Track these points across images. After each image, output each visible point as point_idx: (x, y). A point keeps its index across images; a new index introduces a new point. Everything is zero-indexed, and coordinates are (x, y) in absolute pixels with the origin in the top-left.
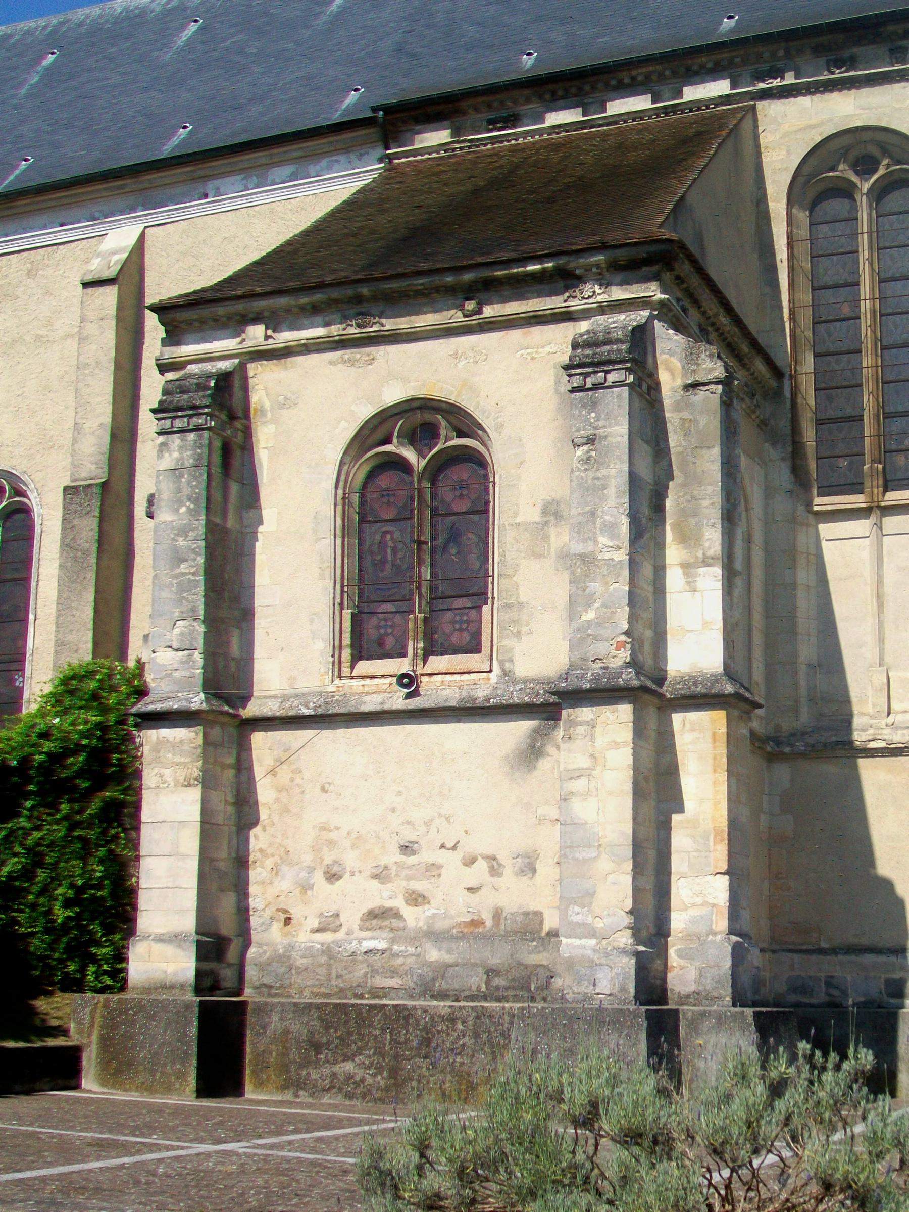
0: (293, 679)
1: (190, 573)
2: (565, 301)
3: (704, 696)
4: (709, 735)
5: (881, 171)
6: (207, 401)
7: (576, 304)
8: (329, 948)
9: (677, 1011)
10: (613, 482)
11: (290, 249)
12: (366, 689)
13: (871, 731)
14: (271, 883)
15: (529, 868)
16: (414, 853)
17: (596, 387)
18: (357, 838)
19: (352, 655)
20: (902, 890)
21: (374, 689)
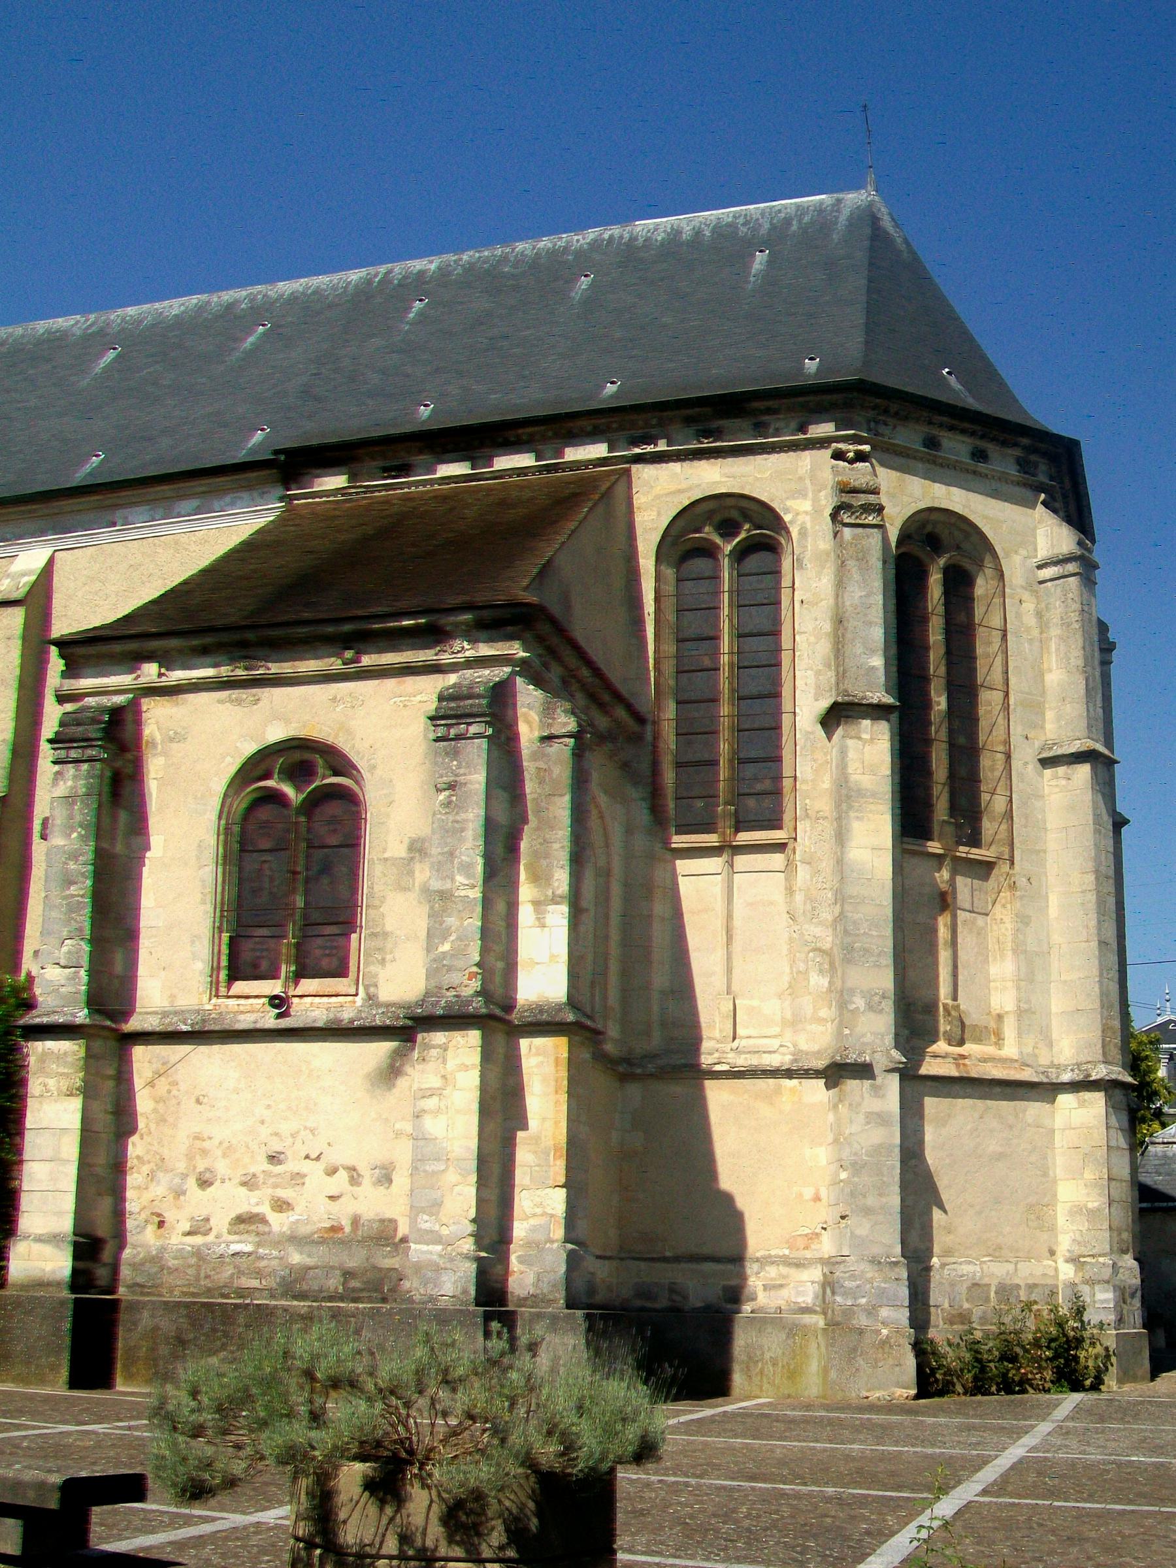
0: (173, 997)
1: (78, 896)
2: (436, 655)
3: (548, 1023)
4: (552, 1060)
5: (743, 535)
6: (99, 735)
7: (446, 658)
8: (199, 1249)
9: (514, 1313)
10: (471, 825)
11: (186, 588)
12: (242, 1008)
13: (716, 1055)
14: (147, 1188)
15: (385, 1178)
16: (280, 1162)
17: (459, 737)
18: (228, 1148)
19: (228, 975)
20: (741, 1203)
21: (249, 1008)
